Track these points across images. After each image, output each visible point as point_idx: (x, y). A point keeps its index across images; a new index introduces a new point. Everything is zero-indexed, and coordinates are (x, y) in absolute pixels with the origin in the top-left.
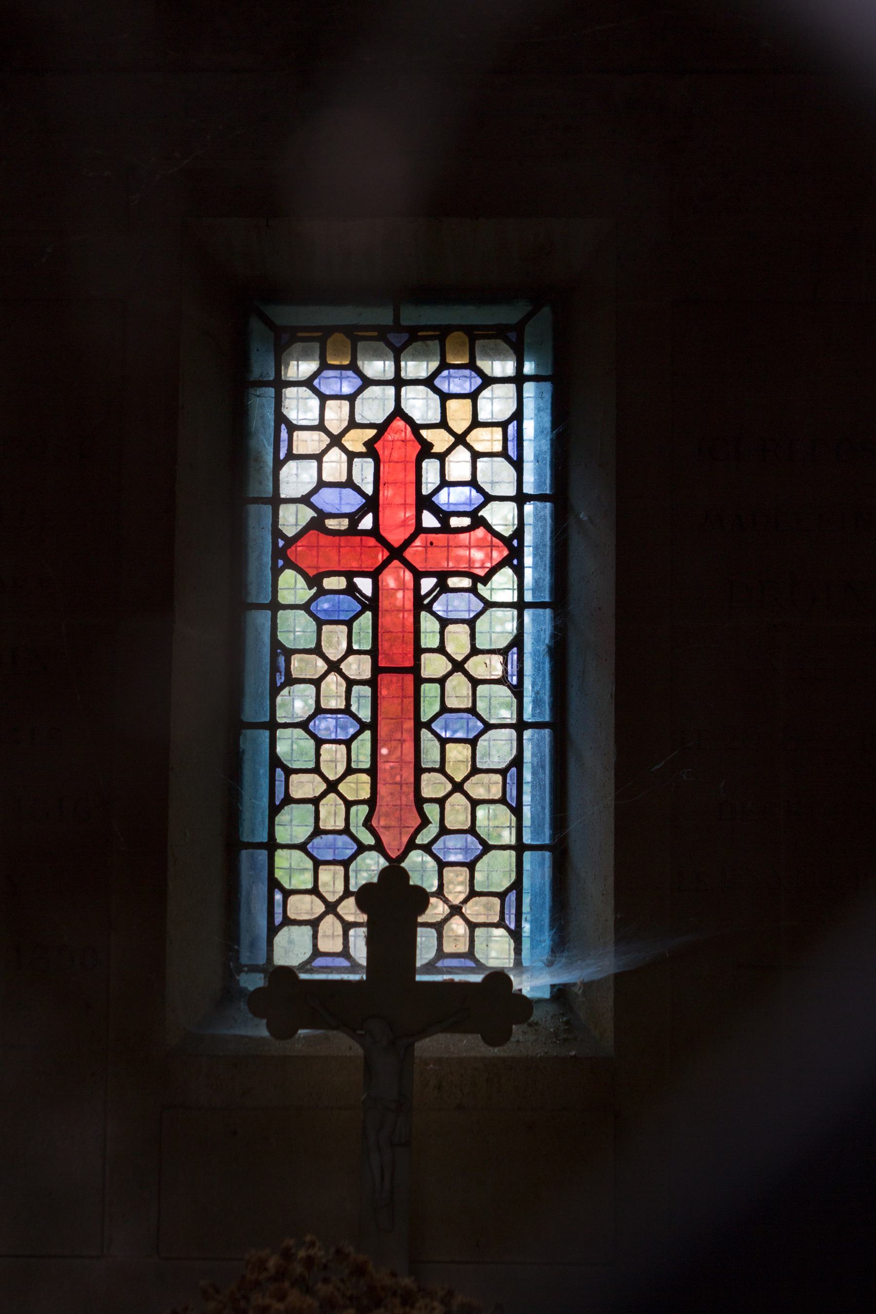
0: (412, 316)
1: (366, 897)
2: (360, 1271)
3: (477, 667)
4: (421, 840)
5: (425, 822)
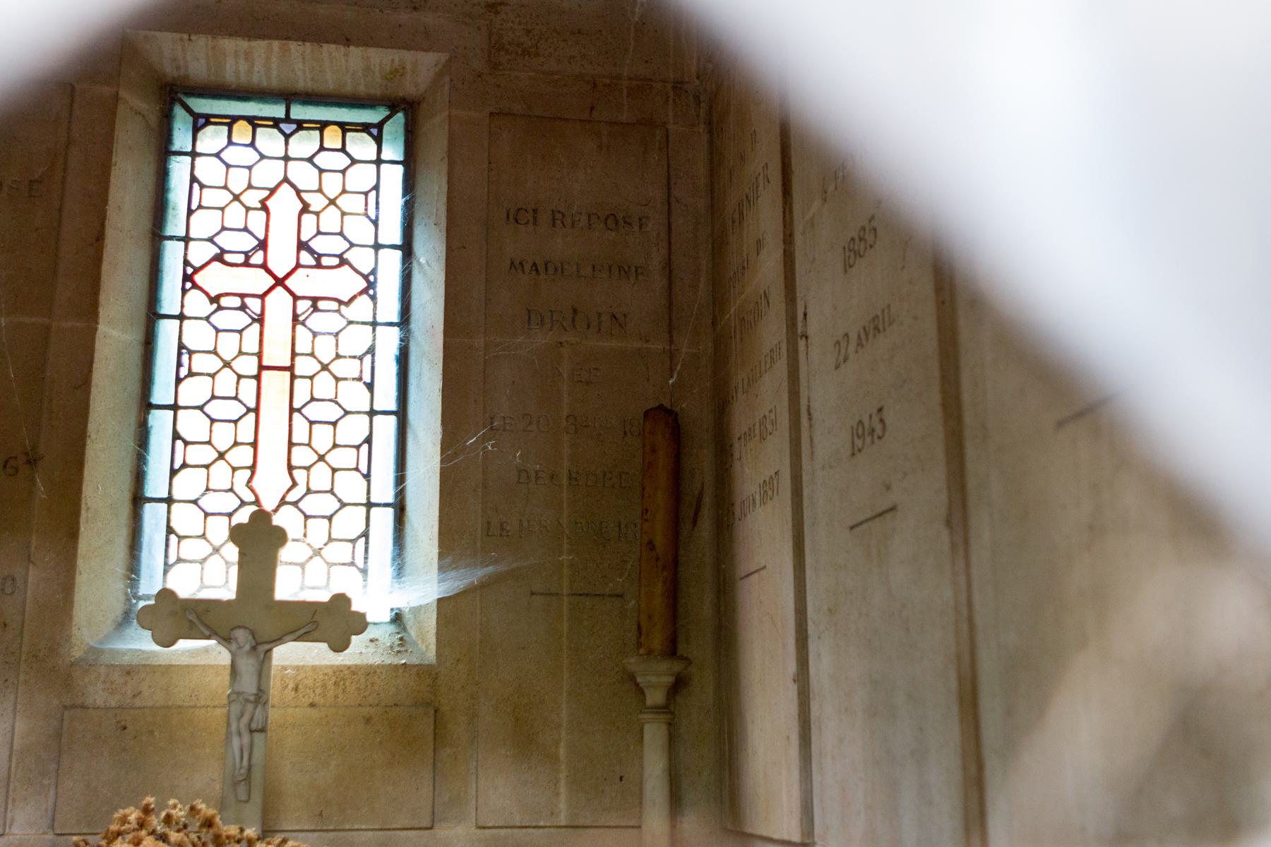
0: (298, 112)
1: (237, 534)
2: (208, 823)
3: (339, 368)
4: (292, 497)
5: (295, 484)
